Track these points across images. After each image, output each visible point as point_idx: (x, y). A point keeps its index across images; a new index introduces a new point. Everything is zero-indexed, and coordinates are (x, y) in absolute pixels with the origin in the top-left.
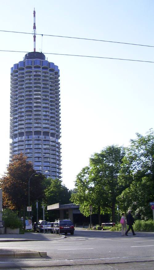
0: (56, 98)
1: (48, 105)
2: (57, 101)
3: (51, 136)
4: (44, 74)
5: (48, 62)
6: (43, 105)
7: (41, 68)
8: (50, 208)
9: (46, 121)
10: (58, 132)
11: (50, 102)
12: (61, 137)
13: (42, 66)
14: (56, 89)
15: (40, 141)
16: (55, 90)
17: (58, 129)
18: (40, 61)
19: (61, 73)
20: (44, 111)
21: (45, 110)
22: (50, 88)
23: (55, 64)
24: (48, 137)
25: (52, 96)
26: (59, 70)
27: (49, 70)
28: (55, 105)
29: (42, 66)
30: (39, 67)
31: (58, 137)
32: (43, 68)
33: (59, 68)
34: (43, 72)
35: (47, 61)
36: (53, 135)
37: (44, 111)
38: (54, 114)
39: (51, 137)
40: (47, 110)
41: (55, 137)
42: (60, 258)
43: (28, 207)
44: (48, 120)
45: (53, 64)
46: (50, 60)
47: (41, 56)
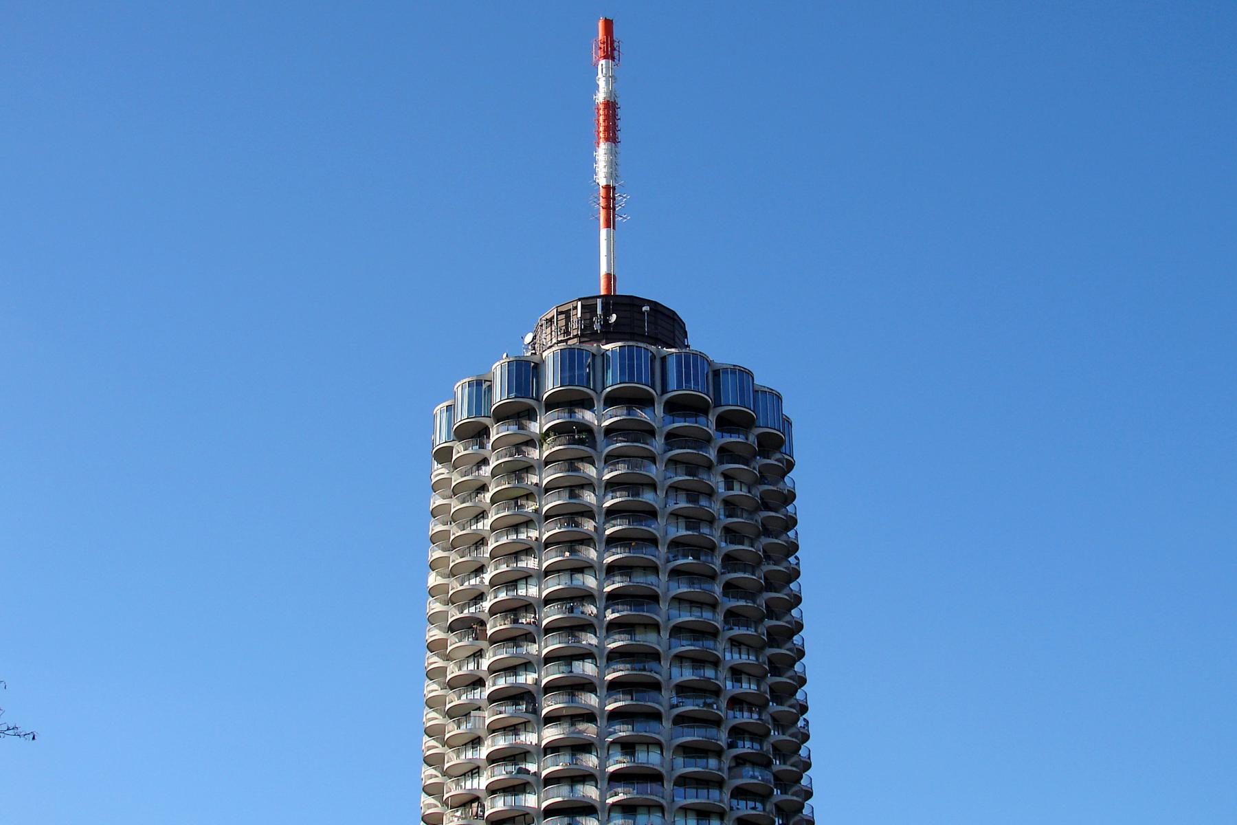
0: (773, 707)
2: (780, 703)
6: (675, 671)
7: (659, 410)
13: (664, 391)
14: (772, 611)
17: (784, 792)
19: (802, 446)
22: (725, 547)
23: (762, 379)
26: (788, 422)
27: (712, 418)
29: (664, 391)
30: (646, 401)
32: (673, 407)
33: (787, 410)
34: (673, 462)
35: (700, 358)
42: (607, 208)
45: (744, 374)
46: (720, 355)
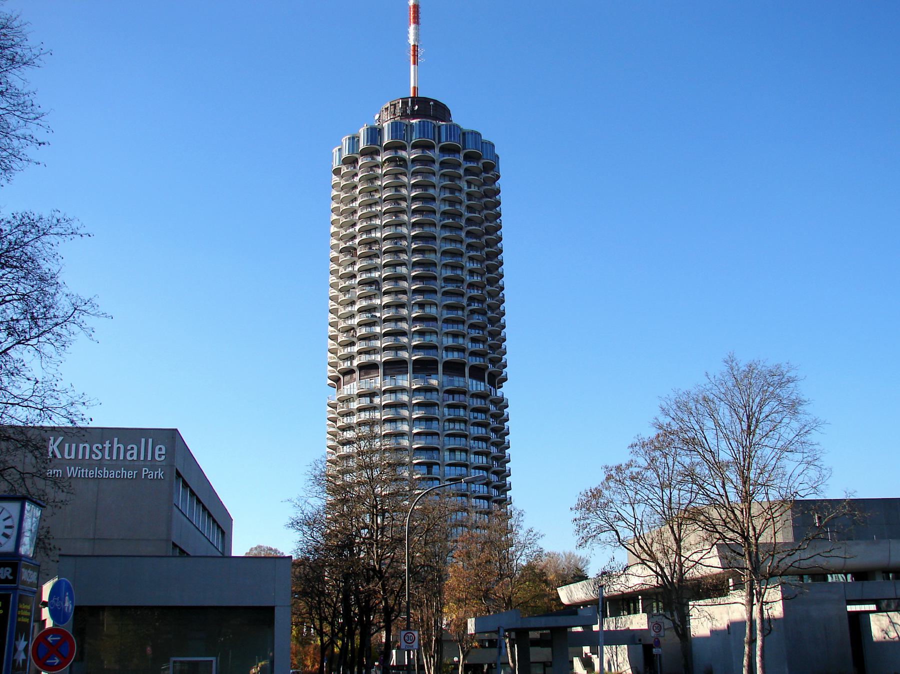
0: (488, 288)
1: (458, 246)
3: (472, 376)
4: (448, 195)
5: (461, 129)
7: (437, 150)
8: (49, 624)
9: (456, 354)
10: (498, 362)
11: (467, 248)
12: (505, 380)
15: (435, 423)
16: (484, 234)
17: (493, 326)
18: (439, 127)
19: (504, 168)
20: (447, 334)
21: (450, 328)
22: (467, 215)
24: (461, 379)
25: (472, 165)
26: (497, 157)
27: (462, 155)
28: (483, 222)
30: (431, 147)
31: (497, 380)
34: (443, 175)
36: (477, 373)
37: (447, 334)
38: (482, 327)
39: (469, 381)
40: (460, 328)
41: (484, 381)
43: (626, 646)
44: (463, 322)
45: (477, 135)
46: (466, 126)
47: (439, 111)
